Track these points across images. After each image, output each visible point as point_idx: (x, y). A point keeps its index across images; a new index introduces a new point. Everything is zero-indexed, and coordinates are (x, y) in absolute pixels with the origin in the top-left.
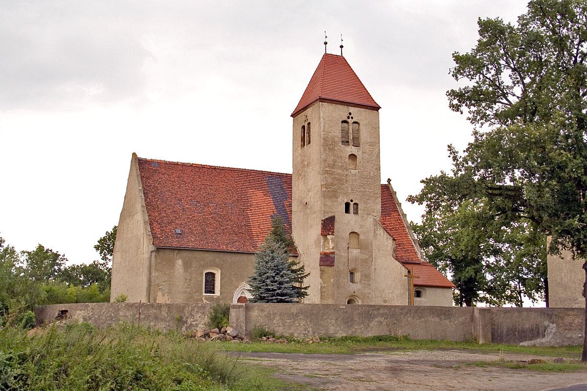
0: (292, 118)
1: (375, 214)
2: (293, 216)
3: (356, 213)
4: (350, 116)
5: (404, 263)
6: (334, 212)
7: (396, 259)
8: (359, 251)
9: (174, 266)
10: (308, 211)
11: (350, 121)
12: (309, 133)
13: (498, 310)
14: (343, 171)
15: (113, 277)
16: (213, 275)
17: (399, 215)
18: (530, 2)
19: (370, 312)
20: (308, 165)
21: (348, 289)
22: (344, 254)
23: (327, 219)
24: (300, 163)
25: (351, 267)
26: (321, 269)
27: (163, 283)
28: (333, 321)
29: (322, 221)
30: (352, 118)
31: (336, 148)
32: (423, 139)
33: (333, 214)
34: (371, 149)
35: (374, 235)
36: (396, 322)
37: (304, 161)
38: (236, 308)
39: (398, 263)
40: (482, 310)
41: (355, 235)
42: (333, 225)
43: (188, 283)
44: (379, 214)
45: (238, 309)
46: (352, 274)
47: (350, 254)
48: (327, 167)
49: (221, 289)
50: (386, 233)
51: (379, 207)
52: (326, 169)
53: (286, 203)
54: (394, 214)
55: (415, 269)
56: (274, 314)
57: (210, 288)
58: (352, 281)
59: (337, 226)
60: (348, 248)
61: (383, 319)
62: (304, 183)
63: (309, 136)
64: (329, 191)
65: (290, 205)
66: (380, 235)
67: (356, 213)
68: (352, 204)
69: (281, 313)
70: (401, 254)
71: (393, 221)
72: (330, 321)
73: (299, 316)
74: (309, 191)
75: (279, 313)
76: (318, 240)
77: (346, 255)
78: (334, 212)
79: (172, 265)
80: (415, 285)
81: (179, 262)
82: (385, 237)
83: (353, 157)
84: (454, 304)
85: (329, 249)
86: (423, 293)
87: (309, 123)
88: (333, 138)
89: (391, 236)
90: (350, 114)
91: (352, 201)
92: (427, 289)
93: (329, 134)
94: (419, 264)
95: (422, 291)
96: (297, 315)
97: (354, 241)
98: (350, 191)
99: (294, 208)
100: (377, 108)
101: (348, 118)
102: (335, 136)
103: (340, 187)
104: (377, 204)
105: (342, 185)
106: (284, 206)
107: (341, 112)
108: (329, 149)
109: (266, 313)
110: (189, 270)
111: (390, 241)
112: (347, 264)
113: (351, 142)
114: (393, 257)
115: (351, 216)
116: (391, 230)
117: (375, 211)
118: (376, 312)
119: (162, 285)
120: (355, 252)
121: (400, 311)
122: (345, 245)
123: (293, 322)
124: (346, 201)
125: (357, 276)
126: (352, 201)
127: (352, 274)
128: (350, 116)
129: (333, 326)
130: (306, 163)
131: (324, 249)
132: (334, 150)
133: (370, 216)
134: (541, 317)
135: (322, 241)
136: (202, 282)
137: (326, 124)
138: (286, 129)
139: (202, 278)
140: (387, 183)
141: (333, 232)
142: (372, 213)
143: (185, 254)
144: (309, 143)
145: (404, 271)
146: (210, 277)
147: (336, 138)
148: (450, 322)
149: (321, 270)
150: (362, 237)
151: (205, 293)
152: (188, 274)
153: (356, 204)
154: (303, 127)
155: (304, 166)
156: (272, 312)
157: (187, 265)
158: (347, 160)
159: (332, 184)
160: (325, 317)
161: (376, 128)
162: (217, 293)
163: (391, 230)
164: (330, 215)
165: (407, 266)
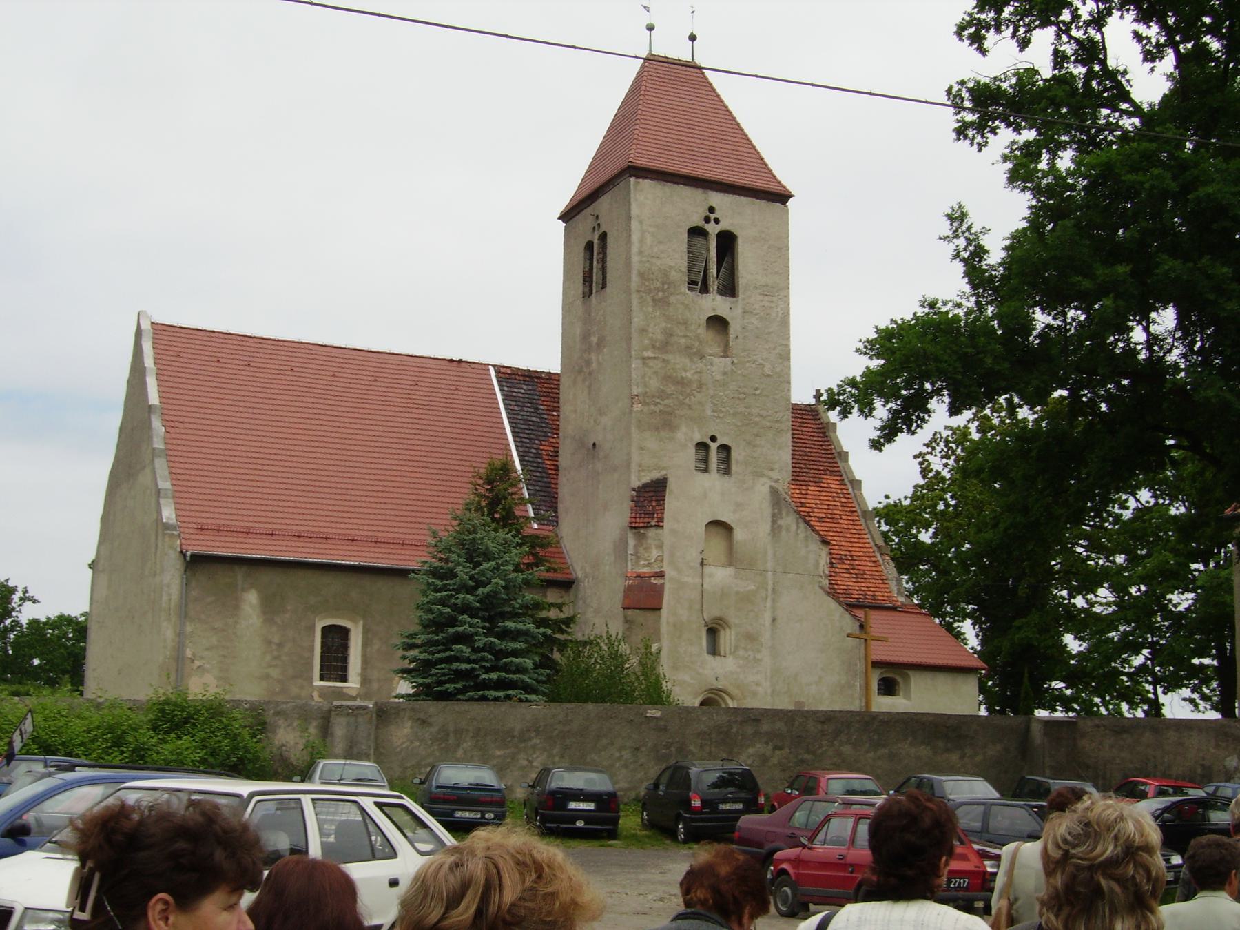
0: (562, 225)
1: (775, 475)
2: (563, 480)
3: (726, 470)
4: (712, 216)
5: (850, 607)
6: (664, 468)
7: (828, 594)
8: (729, 571)
9: (237, 607)
10: (599, 466)
11: (713, 229)
12: (603, 261)
13: (1098, 726)
14: (692, 360)
15: (93, 635)
16: (344, 633)
17: (842, 483)
18: (1141, 56)
19: (734, 730)
20: (600, 345)
21: (701, 671)
22: (691, 579)
23: (646, 486)
24: (582, 337)
25: (711, 612)
26: (625, 617)
27: (207, 653)
28: (626, 754)
29: (634, 490)
30: (717, 221)
31: (672, 299)
32: (892, 212)
33: (663, 472)
34: (767, 304)
35: (773, 529)
36: (806, 756)
37: (589, 335)
38: (348, 714)
39: (833, 604)
40: (1047, 723)
41: (721, 530)
42: (661, 500)
43: (275, 653)
44: (787, 475)
45: (352, 719)
46: (712, 632)
47: (707, 580)
48: (646, 349)
49: (364, 669)
50: (802, 525)
51: (785, 456)
52: (646, 354)
53: (545, 448)
54: (831, 481)
55: (877, 621)
56: (459, 732)
57: (335, 665)
58: (714, 650)
59: (672, 503)
60: (702, 564)
61: (770, 747)
62: (589, 393)
63: (604, 270)
64: (653, 413)
65: (555, 454)
66: (788, 530)
67: (726, 470)
68: (714, 446)
69: (479, 730)
70: (847, 582)
71: (826, 497)
72: (617, 754)
73: (530, 739)
74: (601, 412)
75: (471, 728)
76: (623, 542)
77: (698, 580)
78: (664, 468)
79: (235, 608)
80: (876, 664)
81: (251, 598)
82: (802, 535)
83: (718, 323)
84: (983, 712)
85: (649, 565)
86: (901, 685)
87: (603, 237)
88: (665, 274)
89: (817, 532)
90: (712, 210)
91: (713, 439)
92: (911, 673)
93: (654, 260)
94: (894, 609)
95: (899, 679)
96: (523, 738)
97: (717, 546)
98: (709, 412)
99: (564, 460)
100: (781, 197)
101: (707, 220)
102: (671, 267)
103: (682, 403)
104: (780, 448)
105: (689, 395)
106: (538, 455)
107: (688, 206)
108: (654, 300)
109: (434, 730)
110: (278, 620)
111: (815, 546)
112: (698, 606)
113: (714, 284)
114: (821, 588)
115: (712, 481)
116: (820, 520)
117: (777, 466)
118: (749, 730)
119: (202, 658)
120: (720, 575)
121: (819, 727)
122: (693, 556)
123: (514, 757)
124: (698, 438)
125: (726, 638)
126: (713, 439)
127: (712, 632)
128: (712, 216)
129: (626, 766)
130: (594, 339)
131: (637, 562)
132: (669, 304)
133: (763, 480)
134: (1217, 746)
135: (632, 542)
136: (312, 650)
137: (647, 235)
138: (546, 253)
139: (313, 641)
140: (813, 401)
141: (661, 520)
142: (766, 472)
143: (266, 576)
144: (604, 286)
145: (849, 624)
146: (336, 640)
147: (673, 273)
148: (962, 757)
149: (627, 621)
150: (739, 534)
151: (322, 679)
152: (274, 629)
153: (725, 449)
154: (589, 246)
155: (589, 350)
156: (451, 728)
157: (270, 607)
158: (702, 331)
159: (662, 394)
160: (605, 741)
161: (779, 248)
162: (353, 683)
163: (820, 520)
164: (656, 475)
165: (860, 613)
